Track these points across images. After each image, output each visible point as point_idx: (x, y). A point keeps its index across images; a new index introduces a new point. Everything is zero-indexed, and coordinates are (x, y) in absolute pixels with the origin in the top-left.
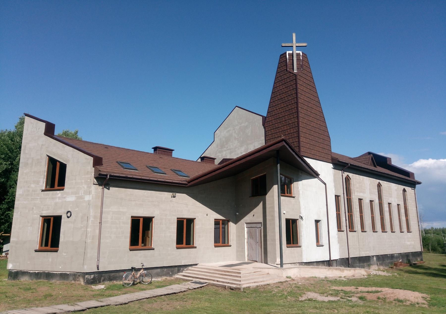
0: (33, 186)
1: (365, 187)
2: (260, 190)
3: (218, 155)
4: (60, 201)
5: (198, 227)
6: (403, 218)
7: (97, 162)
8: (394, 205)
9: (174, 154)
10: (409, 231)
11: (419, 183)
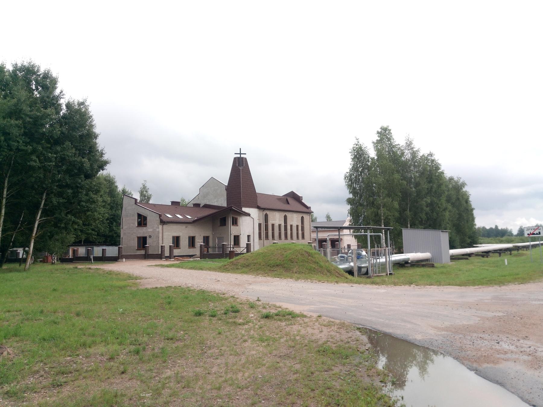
0: (132, 225)
1: (276, 219)
2: (223, 222)
6: (300, 232)
7: (160, 216)
10: (303, 237)
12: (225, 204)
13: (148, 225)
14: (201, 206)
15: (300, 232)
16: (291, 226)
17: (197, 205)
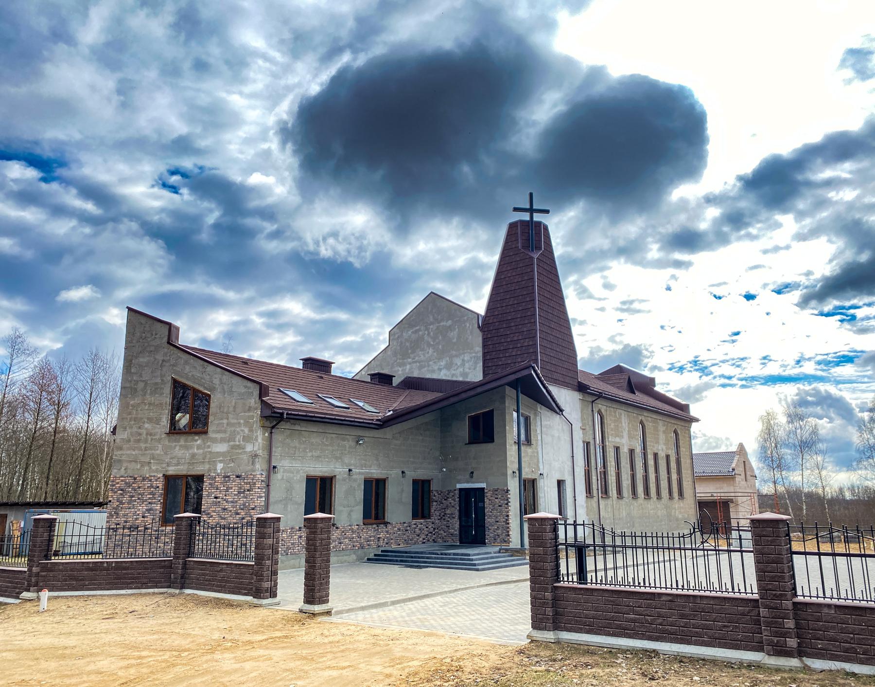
0: (146, 425)
2: (484, 430)
3: (396, 369)
4: (201, 451)
5: (391, 492)
6: (674, 477)
7: (263, 391)
8: (662, 455)
9: (335, 371)
11: (697, 420)
12: (476, 375)
13: (211, 428)
14: (396, 381)
15: (674, 477)
16: (656, 455)
17: (382, 379)
